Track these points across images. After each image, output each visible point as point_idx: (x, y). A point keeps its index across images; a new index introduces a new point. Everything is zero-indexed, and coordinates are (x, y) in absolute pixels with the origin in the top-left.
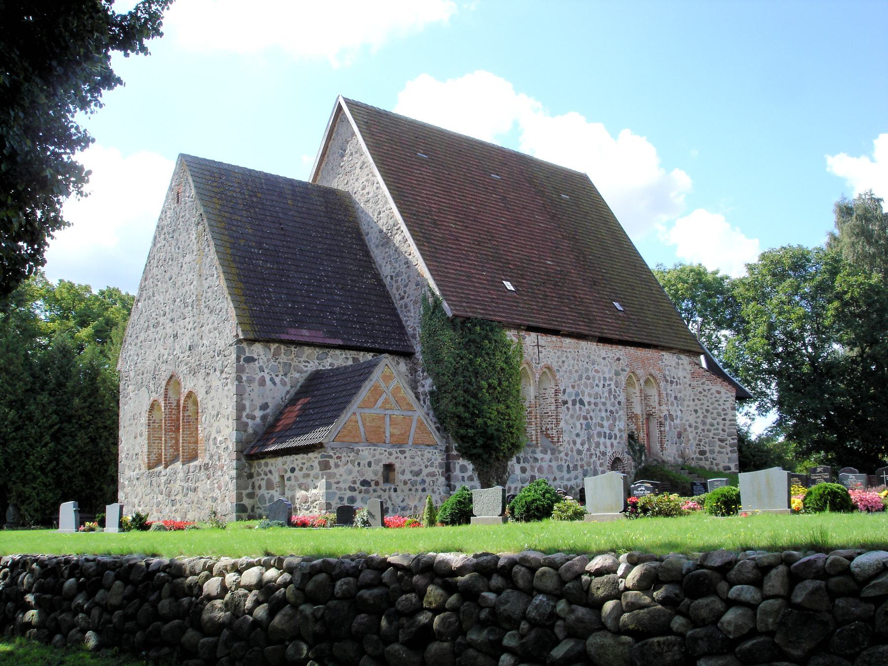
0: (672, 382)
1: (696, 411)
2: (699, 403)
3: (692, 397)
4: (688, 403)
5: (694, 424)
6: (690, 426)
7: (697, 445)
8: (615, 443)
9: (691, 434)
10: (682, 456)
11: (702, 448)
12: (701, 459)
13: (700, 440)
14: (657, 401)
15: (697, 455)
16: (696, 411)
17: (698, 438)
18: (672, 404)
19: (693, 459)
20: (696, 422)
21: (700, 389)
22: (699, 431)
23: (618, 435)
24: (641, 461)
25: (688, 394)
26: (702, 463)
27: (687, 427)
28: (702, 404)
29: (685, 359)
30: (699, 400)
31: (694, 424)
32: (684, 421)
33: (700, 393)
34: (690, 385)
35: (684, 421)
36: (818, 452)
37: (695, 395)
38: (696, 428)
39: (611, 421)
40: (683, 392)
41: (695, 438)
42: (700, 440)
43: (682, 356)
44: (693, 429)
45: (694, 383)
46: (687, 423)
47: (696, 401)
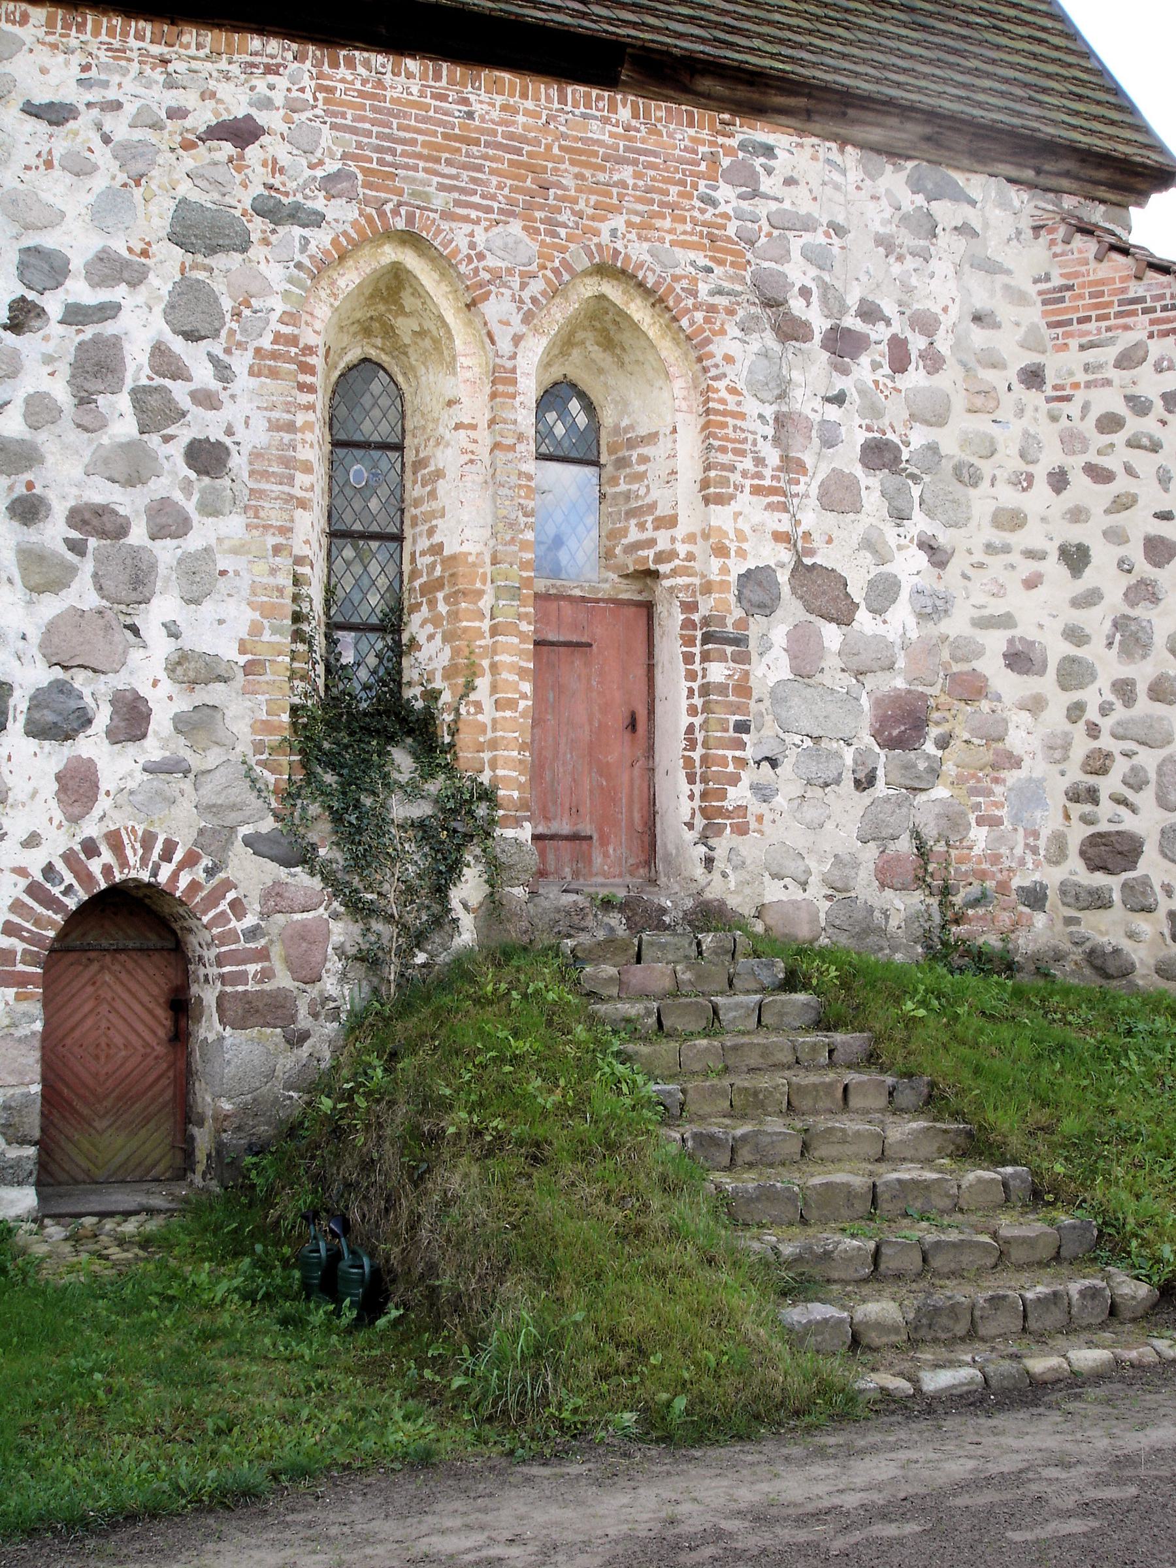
0: (843, 345)
1: (1076, 558)
2: (1096, 497)
3: (1051, 457)
4: (1009, 497)
5: (1057, 649)
6: (1020, 659)
7: (1075, 796)
8: (118, 768)
9: (1030, 727)
10: (925, 867)
11: (1107, 818)
12: (1099, 901)
13: (1099, 764)
14: (689, 467)
15: (1075, 869)
16: (1076, 558)
17: (1082, 746)
18: (839, 497)
19: (1035, 898)
20: (1075, 635)
21: (1110, 401)
22: (1091, 696)
23: (165, 703)
24: (442, 920)
25: (1008, 440)
26: (1106, 929)
27: (992, 667)
28: (1124, 503)
29: (996, 208)
30: (1099, 475)
31: (1057, 649)
32: (956, 625)
33: (1110, 423)
34: (1033, 377)
35: (956, 625)
36: (595, 1012)
37: (1071, 441)
38: (1073, 674)
39: (82, 594)
40: (961, 423)
41: (1058, 749)
42: (1099, 764)
43: (976, 184)
44: (1046, 685)
45: (1064, 364)
46: (996, 642)
47: (1079, 482)
